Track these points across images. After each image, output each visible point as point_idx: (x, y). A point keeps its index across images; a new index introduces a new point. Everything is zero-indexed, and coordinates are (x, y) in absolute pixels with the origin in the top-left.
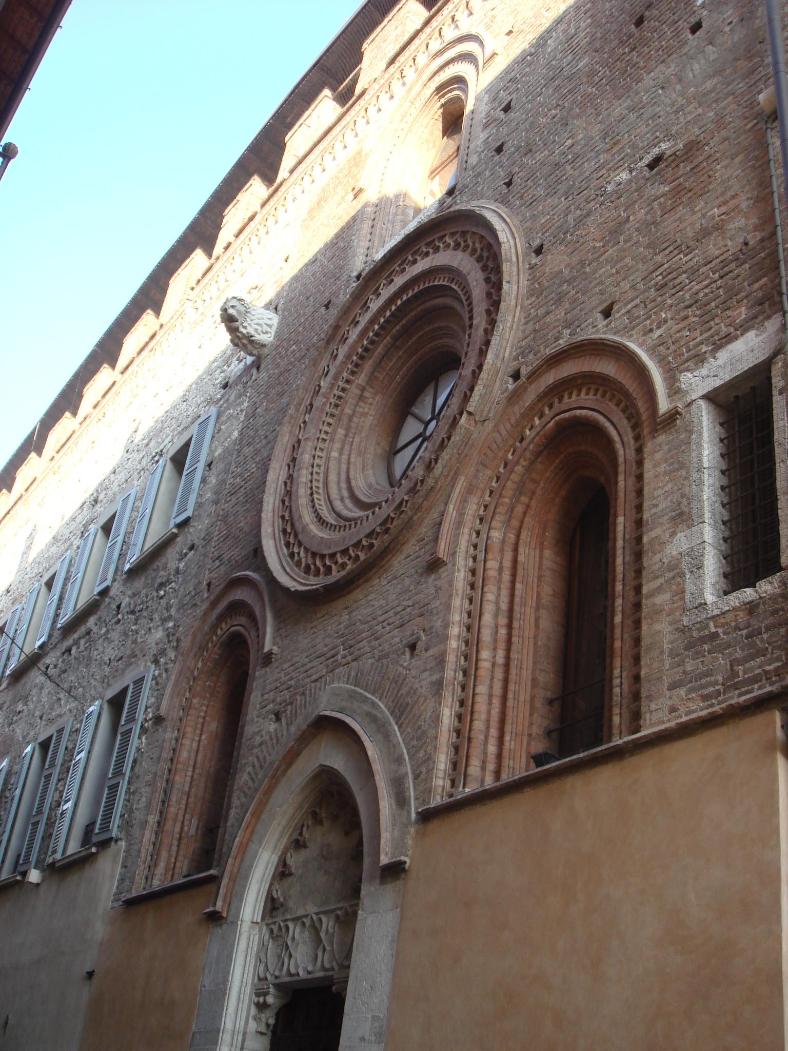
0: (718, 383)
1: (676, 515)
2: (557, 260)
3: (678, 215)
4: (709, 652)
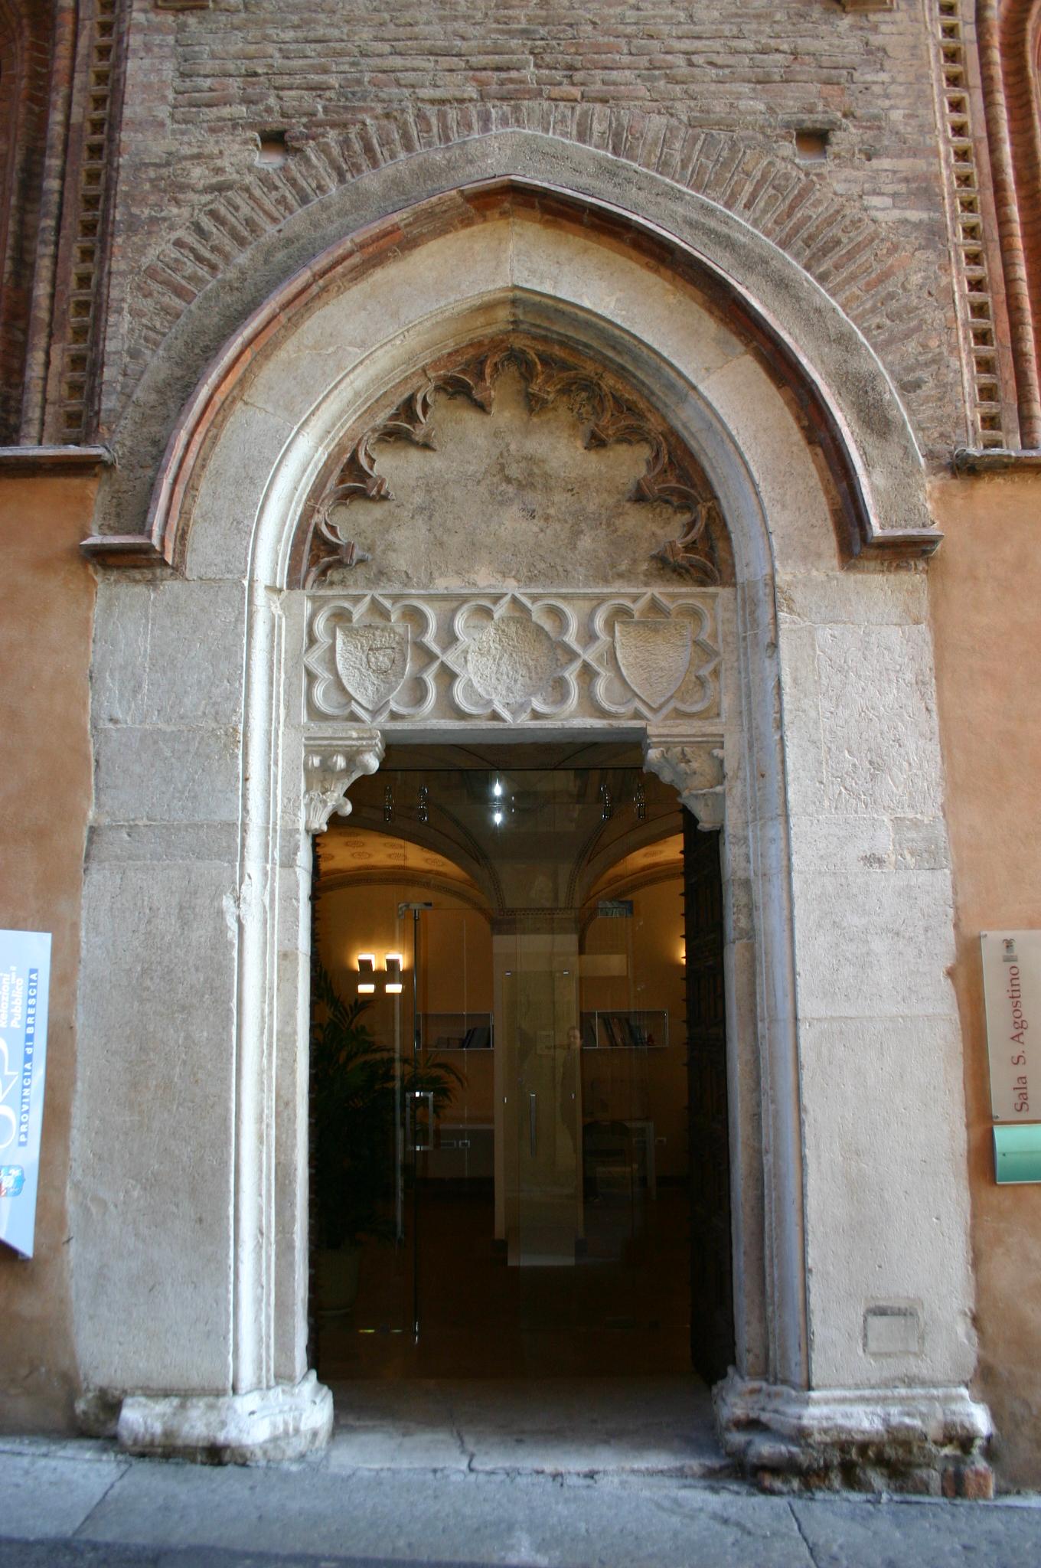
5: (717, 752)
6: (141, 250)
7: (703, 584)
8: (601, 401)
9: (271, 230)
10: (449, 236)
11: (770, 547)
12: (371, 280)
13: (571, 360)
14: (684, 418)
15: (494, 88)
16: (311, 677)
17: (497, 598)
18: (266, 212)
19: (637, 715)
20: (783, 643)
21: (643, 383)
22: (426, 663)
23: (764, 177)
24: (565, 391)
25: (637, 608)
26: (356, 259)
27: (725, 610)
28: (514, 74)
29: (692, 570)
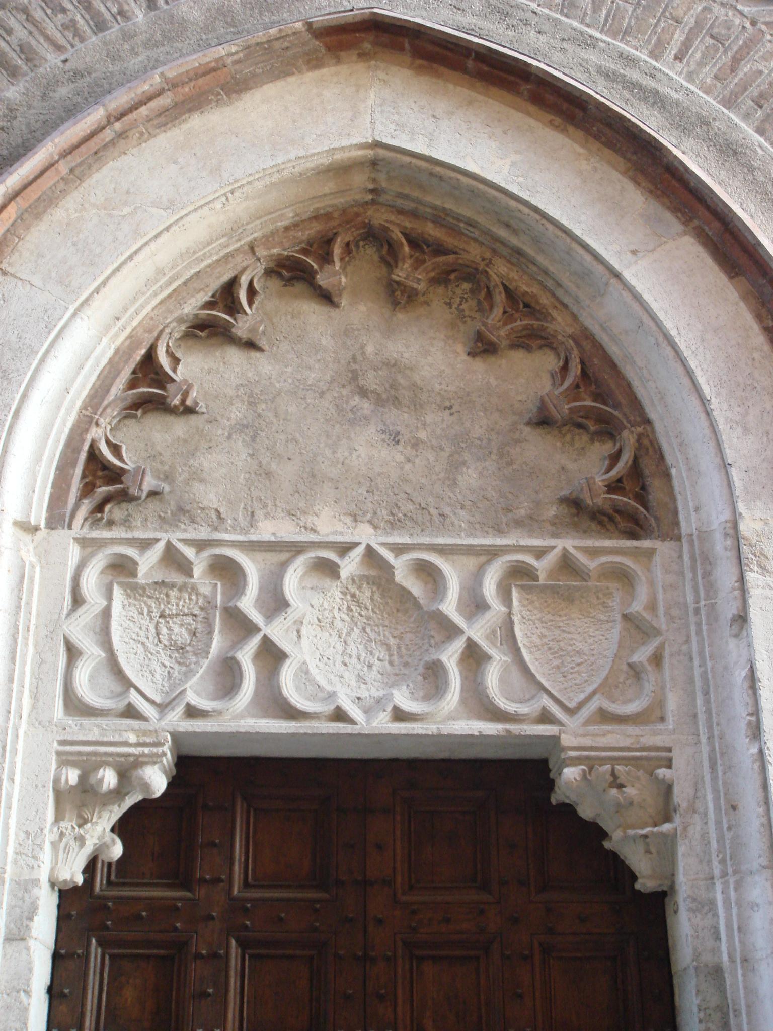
5: (662, 772)
7: (633, 536)
8: (489, 295)
9: (53, 59)
10: (291, 79)
11: (730, 485)
12: (185, 127)
13: (450, 241)
14: (604, 317)
16: (73, 653)
17: (345, 549)
18: (47, 38)
19: (545, 717)
20: (755, 615)
21: (546, 272)
22: (242, 640)
23: (699, 24)
24: (442, 279)
25: (542, 566)
26: (165, 100)
27: (667, 572)
29: (618, 518)
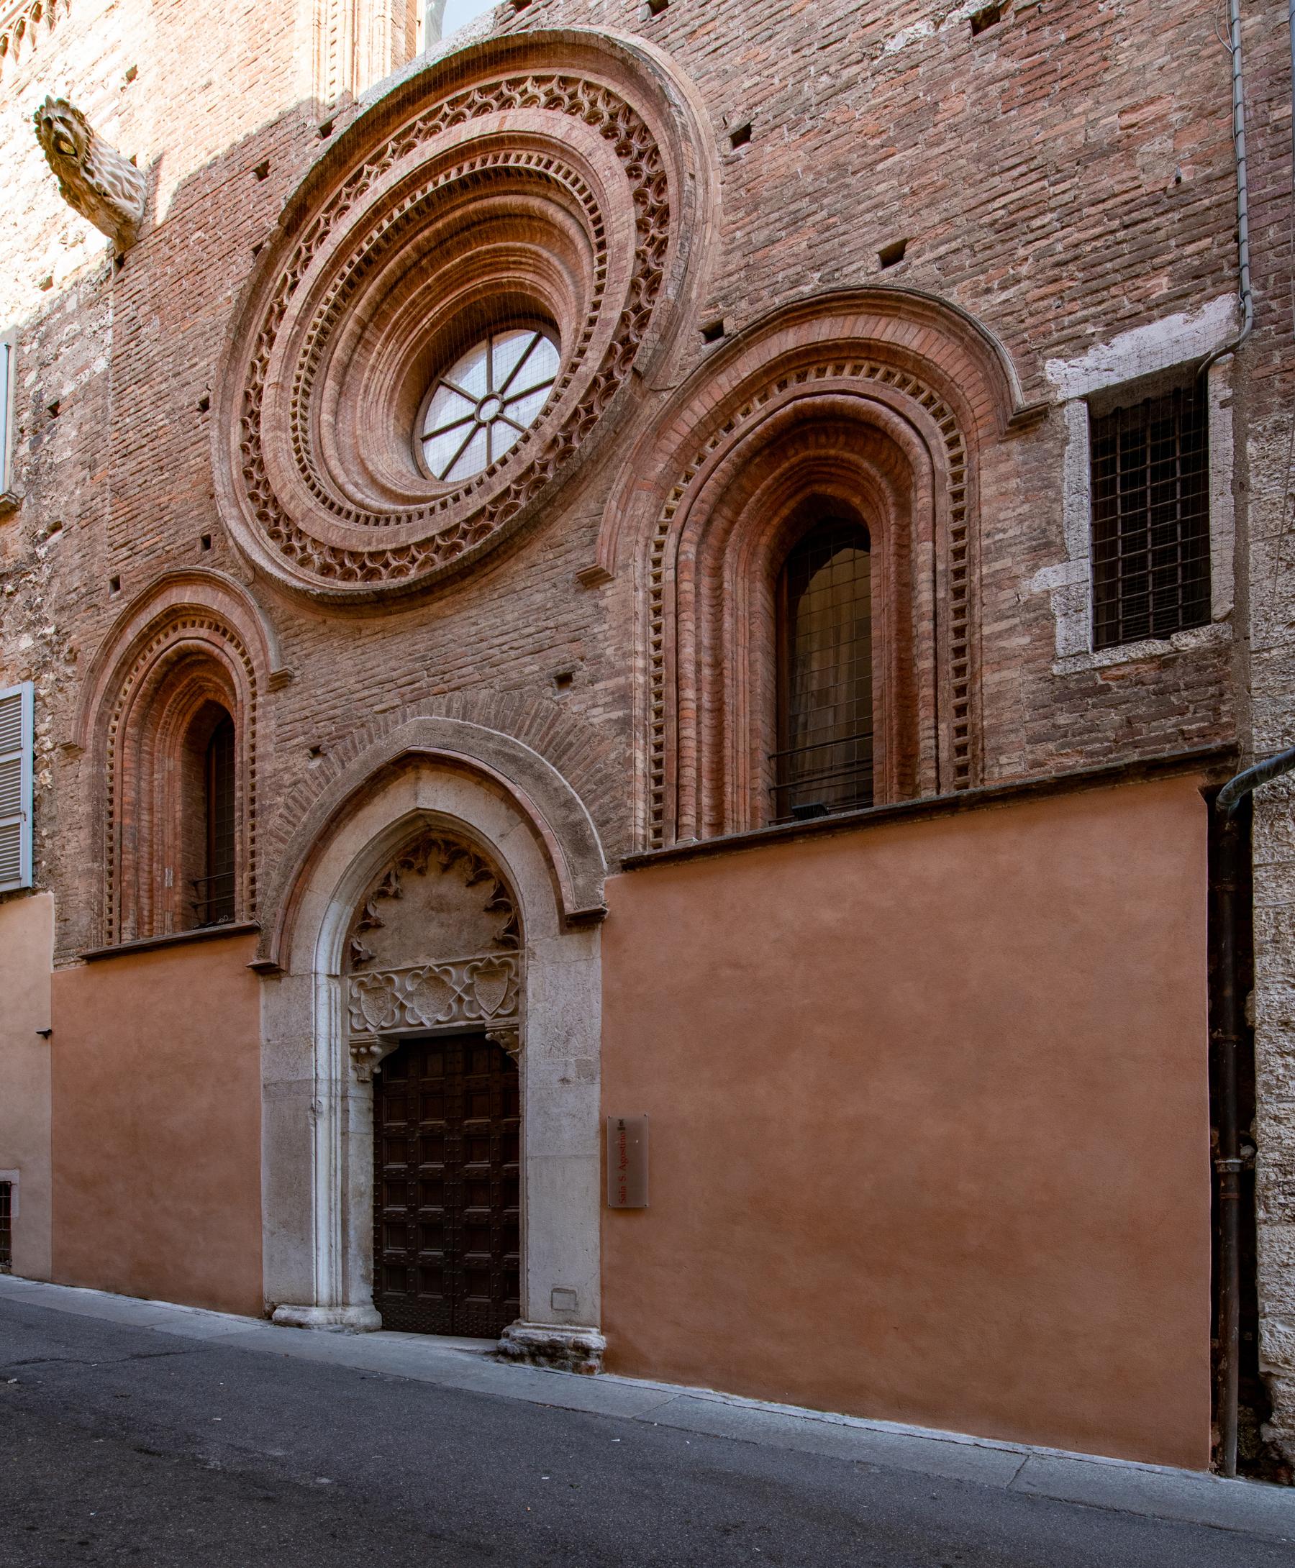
0: (1114, 380)
1: (1039, 545)
2: (778, 156)
3: (1040, 115)
4: (1094, 706)
6: (267, 822)
13: (456, 840)
15: (407, 697)
28: (417, 685)
